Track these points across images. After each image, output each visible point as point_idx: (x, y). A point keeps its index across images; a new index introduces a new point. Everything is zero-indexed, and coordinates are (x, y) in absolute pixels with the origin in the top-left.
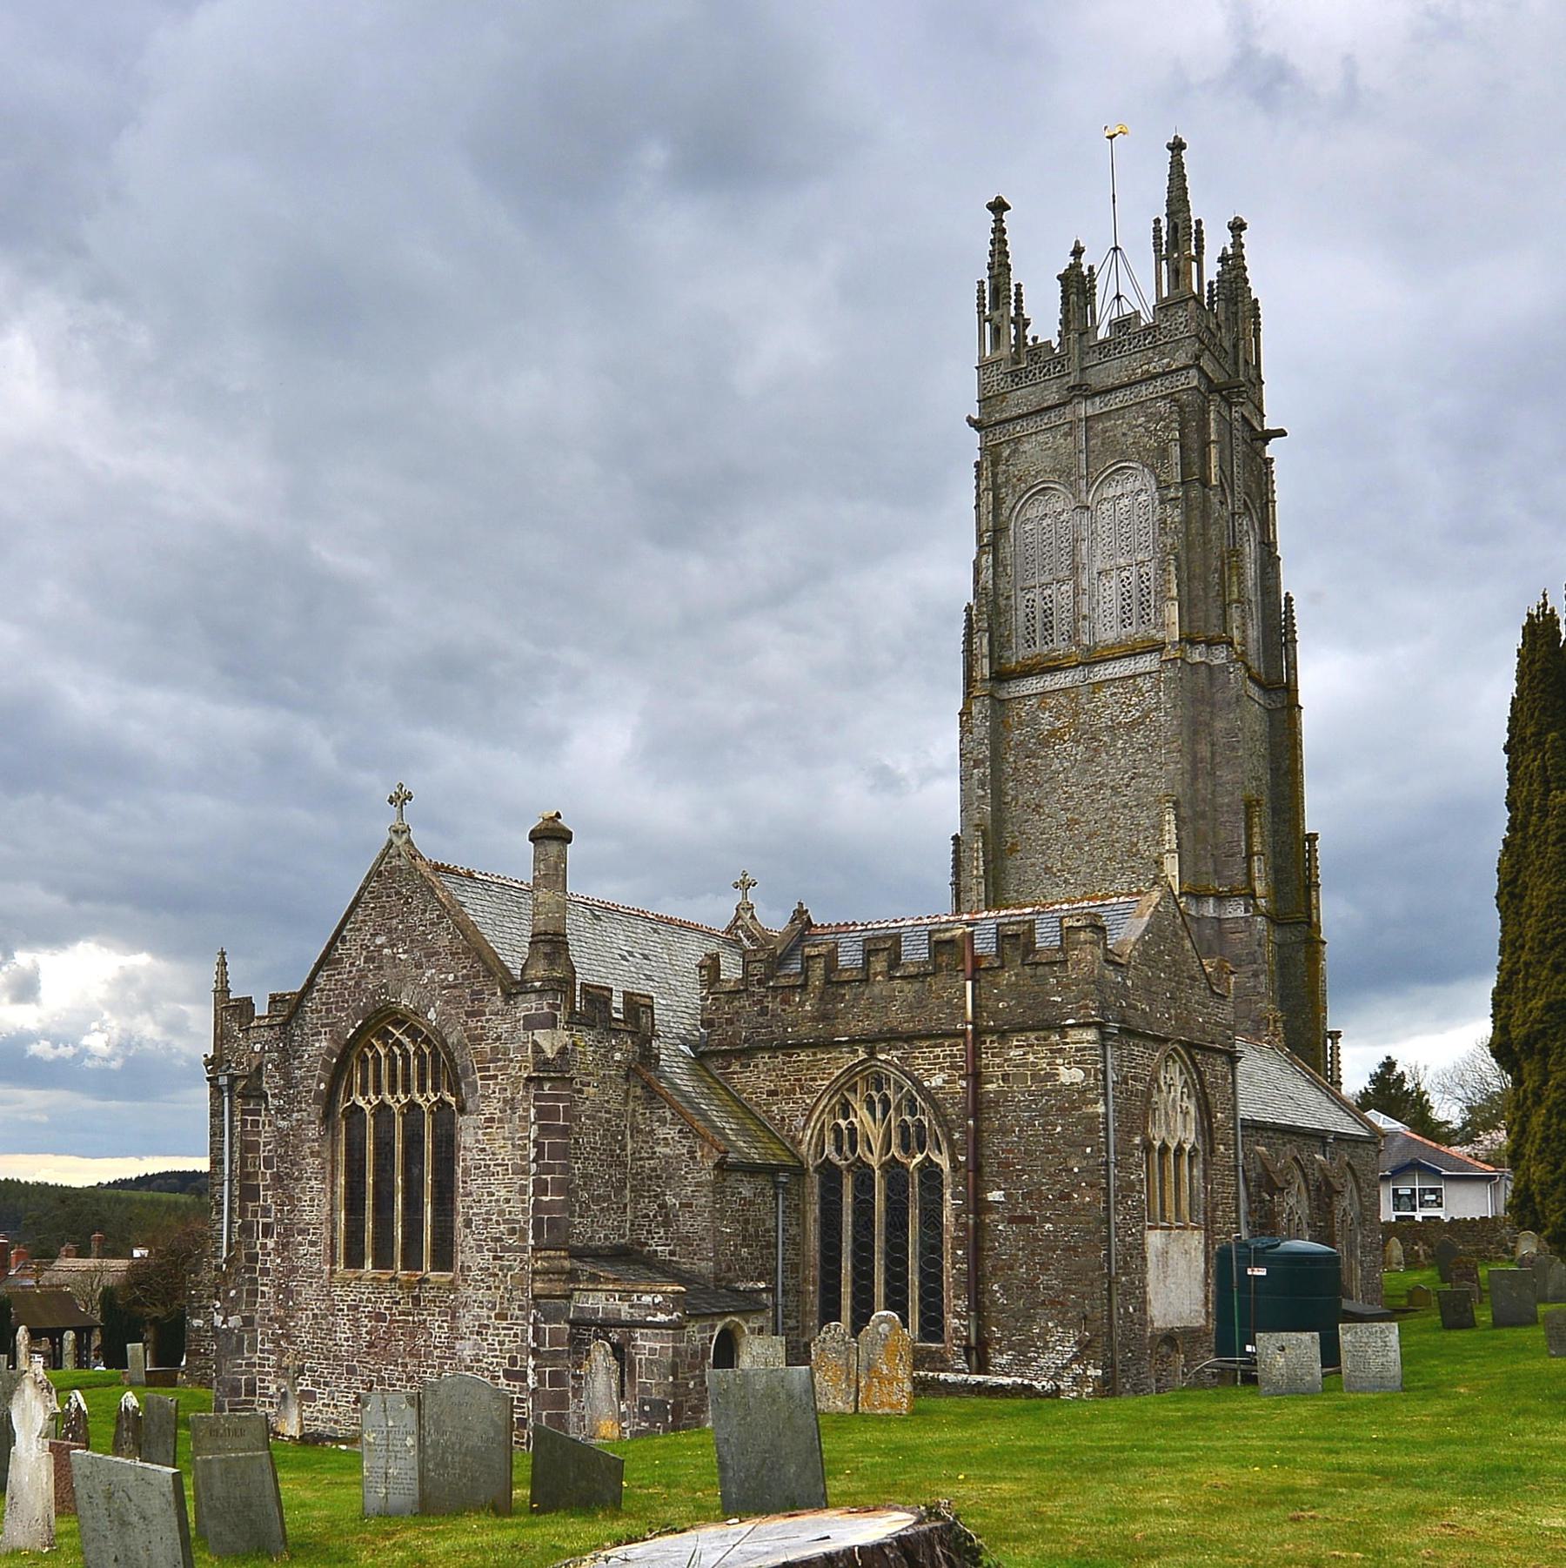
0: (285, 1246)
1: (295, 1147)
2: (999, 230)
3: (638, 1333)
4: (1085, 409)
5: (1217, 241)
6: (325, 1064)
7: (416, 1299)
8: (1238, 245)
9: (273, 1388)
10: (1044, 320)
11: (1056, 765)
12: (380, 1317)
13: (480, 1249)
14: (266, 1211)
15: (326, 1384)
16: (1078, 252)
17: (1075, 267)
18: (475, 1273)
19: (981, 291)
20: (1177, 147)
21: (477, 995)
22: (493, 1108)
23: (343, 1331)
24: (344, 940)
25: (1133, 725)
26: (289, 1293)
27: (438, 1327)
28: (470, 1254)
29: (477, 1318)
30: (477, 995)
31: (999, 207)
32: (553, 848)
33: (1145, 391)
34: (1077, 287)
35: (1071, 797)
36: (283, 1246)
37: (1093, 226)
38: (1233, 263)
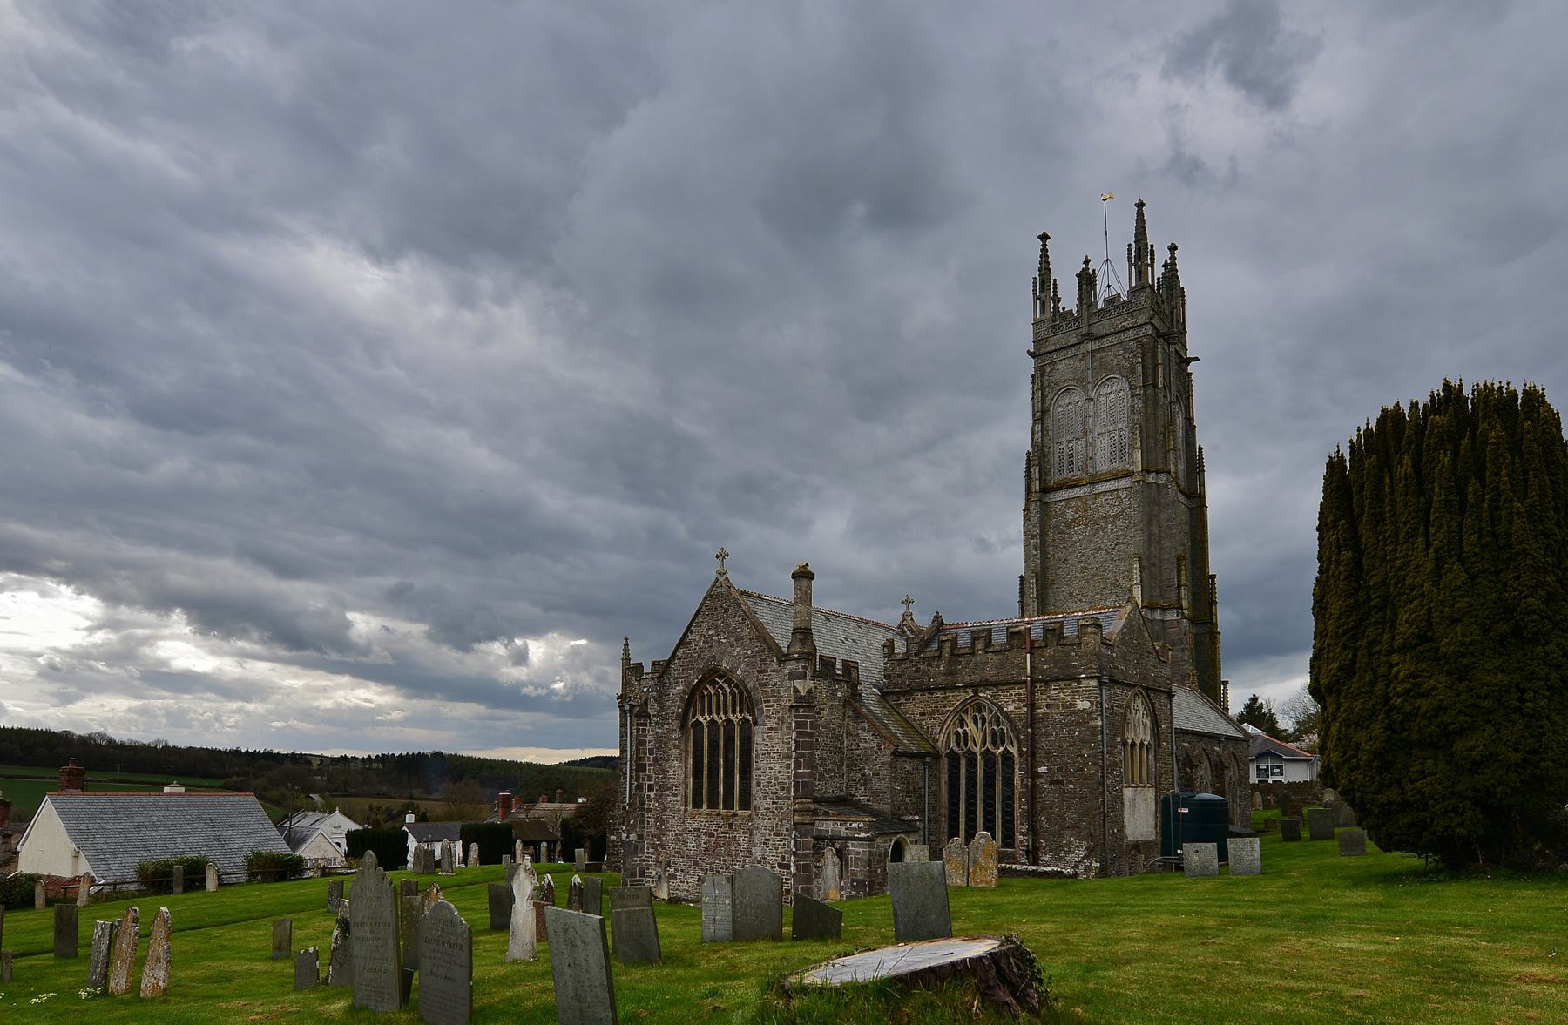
2: (1044, 250)
4: (1091, 346)
5: (1162, 256)
8: (1173, 258)
10: (1069, 299)
12: (711, 835)
14: (650, 778)
16: (1087, 262)
17: (1086, 270)
19: (1130, 250)
20: (1140, 205)
22: (772, 722)
28: (760, 801)
30: (763, 662)
31: (1044, 238)
32: (804, 582)
33: (1123, 337)
34: (1086, 280)
36: (659, 797)
37: (1097, 250)
38: (1170, 268)
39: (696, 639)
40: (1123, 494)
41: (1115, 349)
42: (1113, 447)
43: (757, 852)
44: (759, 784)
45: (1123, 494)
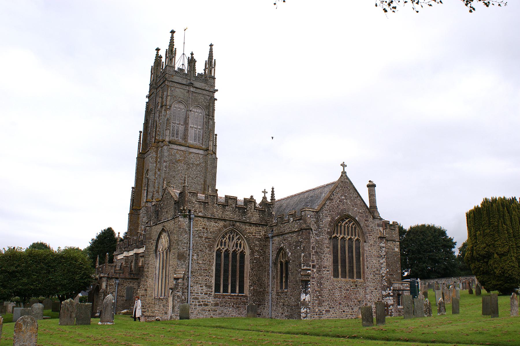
0: (319, 271)
1: (322, 245)
2: (172, 37)
3: (404, 292)
4: (192, 89)
6: (330, 225)
7: (356, 285)
9: (317, 310)
12: (347, 290)
13: (371, 274)
14: (313, 261)
15: (333, 308)
20: (211, 45)
21: (367, 216)
22: (372, 242)
23: (337, 294)
24: (333, 195)
25: (197, 165)
26: (321, 284)
28: (369, 274)
29: (370, 289)
30: (367, 216)
31: (173, 32)
33: (204, 92)
35: (182, 177)
36: (319, 271)
39: (336, 198)
41: (201, 95)
42: (195, 134)
44: (368, 268)
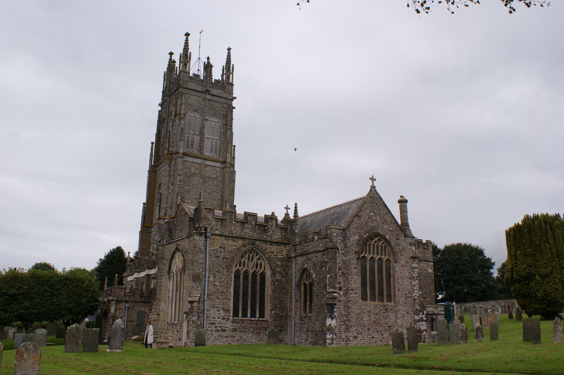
0: (347, 294)
2: (187, 41)
3: (438, 316)
4: (208, 97)
6: (358, 244)
7: (386, 309)
9: (344, 336)
11: (194, 182)
12: (377, 314)
14: (340, 283)
15: (361, 333)
18: (401, 303)
20: (229, 49)
22: (403, 262)
23: (366, 318)
24: (361, 211)
25: (214, 179)
26: (348, 308)
27: (392, 315)
29: (402, 314)
30: (398, 235)
31: (187, 35)
32: (403, 204)
33: (222, 100)
36: (346, 294)
40: (218, 170)
43: (399, 321)
44: (399, 290)
45: (218, 170)
